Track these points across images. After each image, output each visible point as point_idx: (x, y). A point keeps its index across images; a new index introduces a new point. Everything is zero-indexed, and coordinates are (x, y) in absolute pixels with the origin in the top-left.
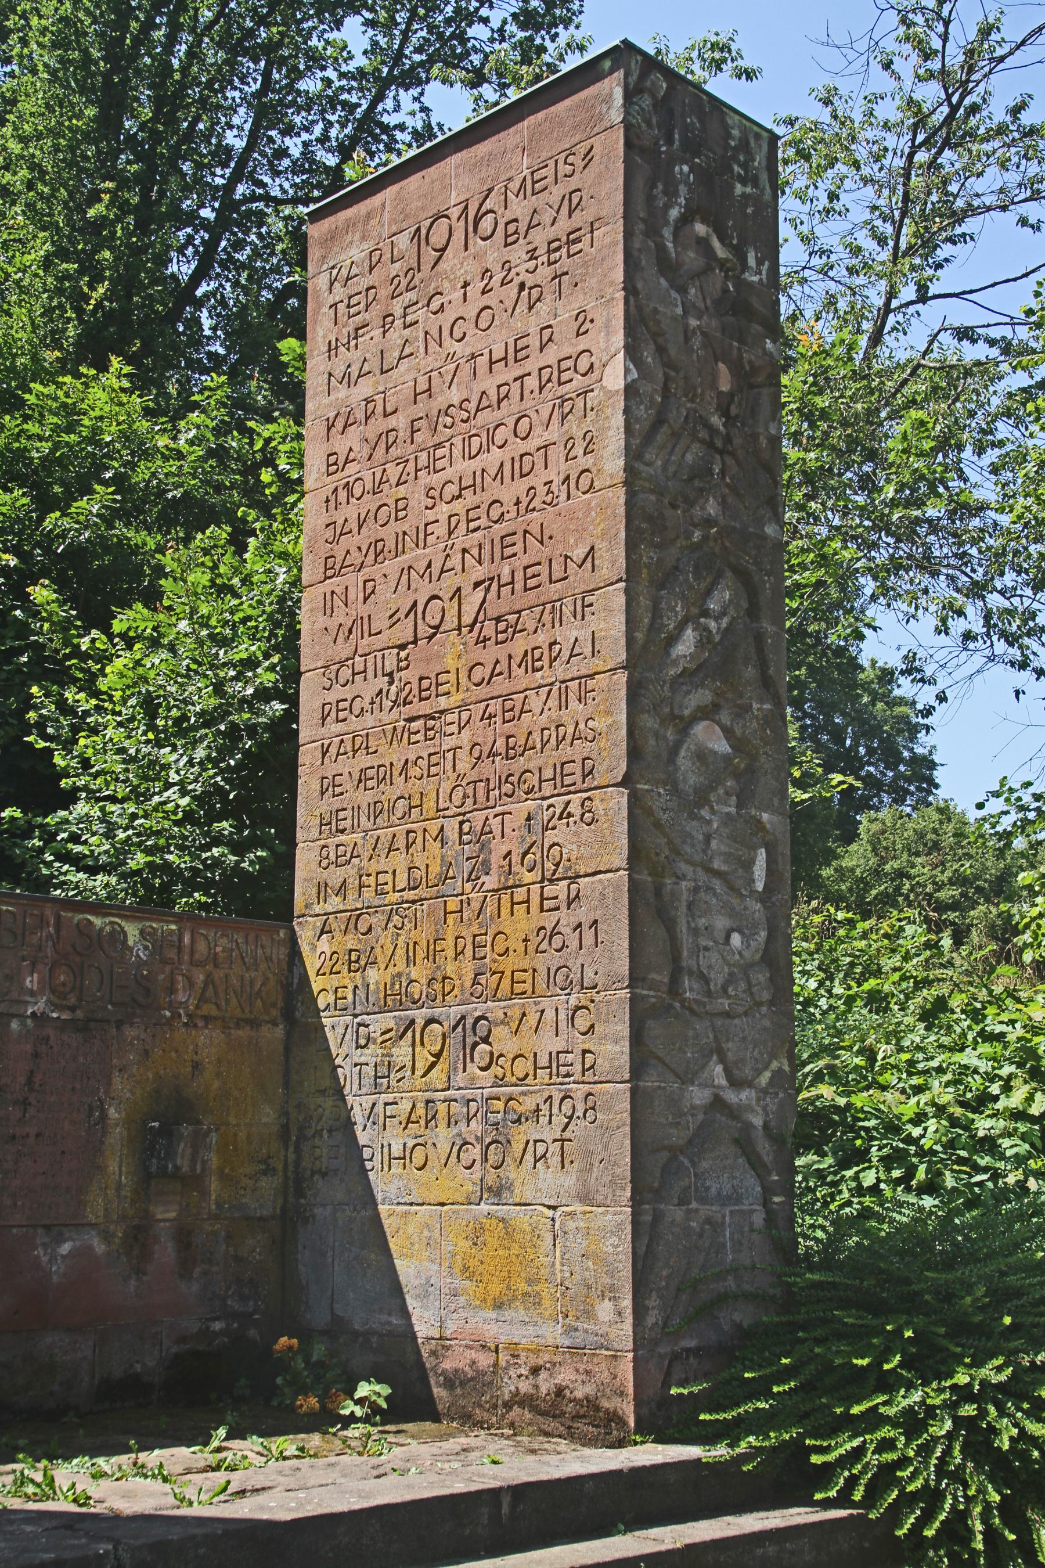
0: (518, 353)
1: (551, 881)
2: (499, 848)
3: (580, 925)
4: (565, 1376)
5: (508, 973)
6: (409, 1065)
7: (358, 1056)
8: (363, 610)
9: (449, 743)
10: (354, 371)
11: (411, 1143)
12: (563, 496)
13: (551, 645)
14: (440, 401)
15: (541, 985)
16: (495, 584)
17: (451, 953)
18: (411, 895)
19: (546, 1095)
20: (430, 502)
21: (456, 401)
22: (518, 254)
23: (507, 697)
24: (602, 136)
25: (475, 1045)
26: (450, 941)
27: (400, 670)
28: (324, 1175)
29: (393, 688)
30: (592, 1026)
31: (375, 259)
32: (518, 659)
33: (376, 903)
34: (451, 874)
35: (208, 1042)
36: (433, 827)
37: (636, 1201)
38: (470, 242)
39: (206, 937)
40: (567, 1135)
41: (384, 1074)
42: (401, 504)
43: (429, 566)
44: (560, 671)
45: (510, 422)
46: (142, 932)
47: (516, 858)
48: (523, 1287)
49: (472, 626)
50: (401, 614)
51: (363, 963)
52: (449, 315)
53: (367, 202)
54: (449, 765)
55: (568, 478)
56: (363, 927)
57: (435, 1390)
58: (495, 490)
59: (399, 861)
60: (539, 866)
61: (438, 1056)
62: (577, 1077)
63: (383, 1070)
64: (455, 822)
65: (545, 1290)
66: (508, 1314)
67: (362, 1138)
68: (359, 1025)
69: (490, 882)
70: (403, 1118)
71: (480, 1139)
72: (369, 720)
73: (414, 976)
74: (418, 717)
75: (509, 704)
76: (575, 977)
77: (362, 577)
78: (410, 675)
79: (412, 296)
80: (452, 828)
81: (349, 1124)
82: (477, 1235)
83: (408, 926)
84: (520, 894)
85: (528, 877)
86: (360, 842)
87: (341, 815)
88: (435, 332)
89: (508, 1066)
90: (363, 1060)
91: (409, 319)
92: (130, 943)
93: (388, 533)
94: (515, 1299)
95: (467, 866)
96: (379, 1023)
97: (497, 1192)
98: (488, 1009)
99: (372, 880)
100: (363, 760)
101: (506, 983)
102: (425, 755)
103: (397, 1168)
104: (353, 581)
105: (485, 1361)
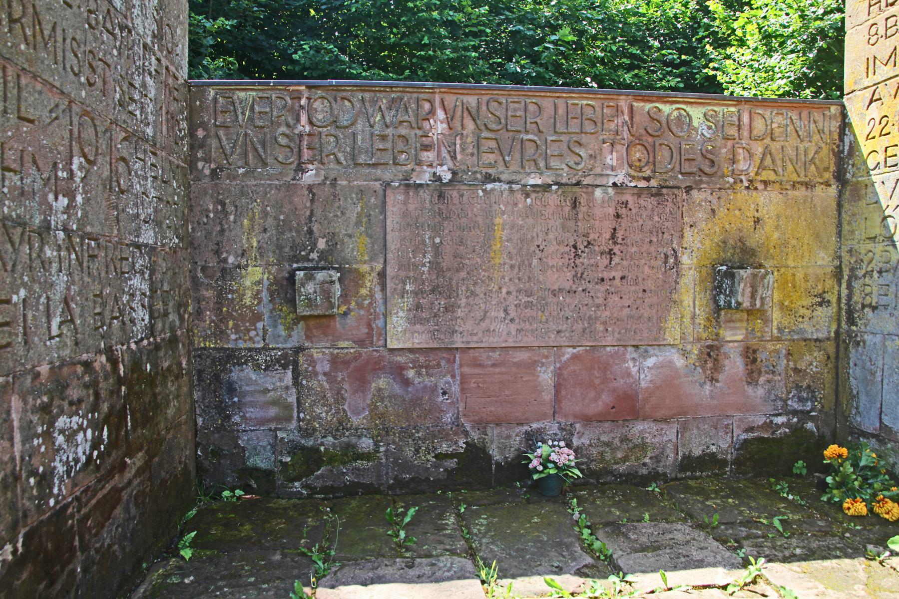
35: (768, 202)
92: (695, 124)
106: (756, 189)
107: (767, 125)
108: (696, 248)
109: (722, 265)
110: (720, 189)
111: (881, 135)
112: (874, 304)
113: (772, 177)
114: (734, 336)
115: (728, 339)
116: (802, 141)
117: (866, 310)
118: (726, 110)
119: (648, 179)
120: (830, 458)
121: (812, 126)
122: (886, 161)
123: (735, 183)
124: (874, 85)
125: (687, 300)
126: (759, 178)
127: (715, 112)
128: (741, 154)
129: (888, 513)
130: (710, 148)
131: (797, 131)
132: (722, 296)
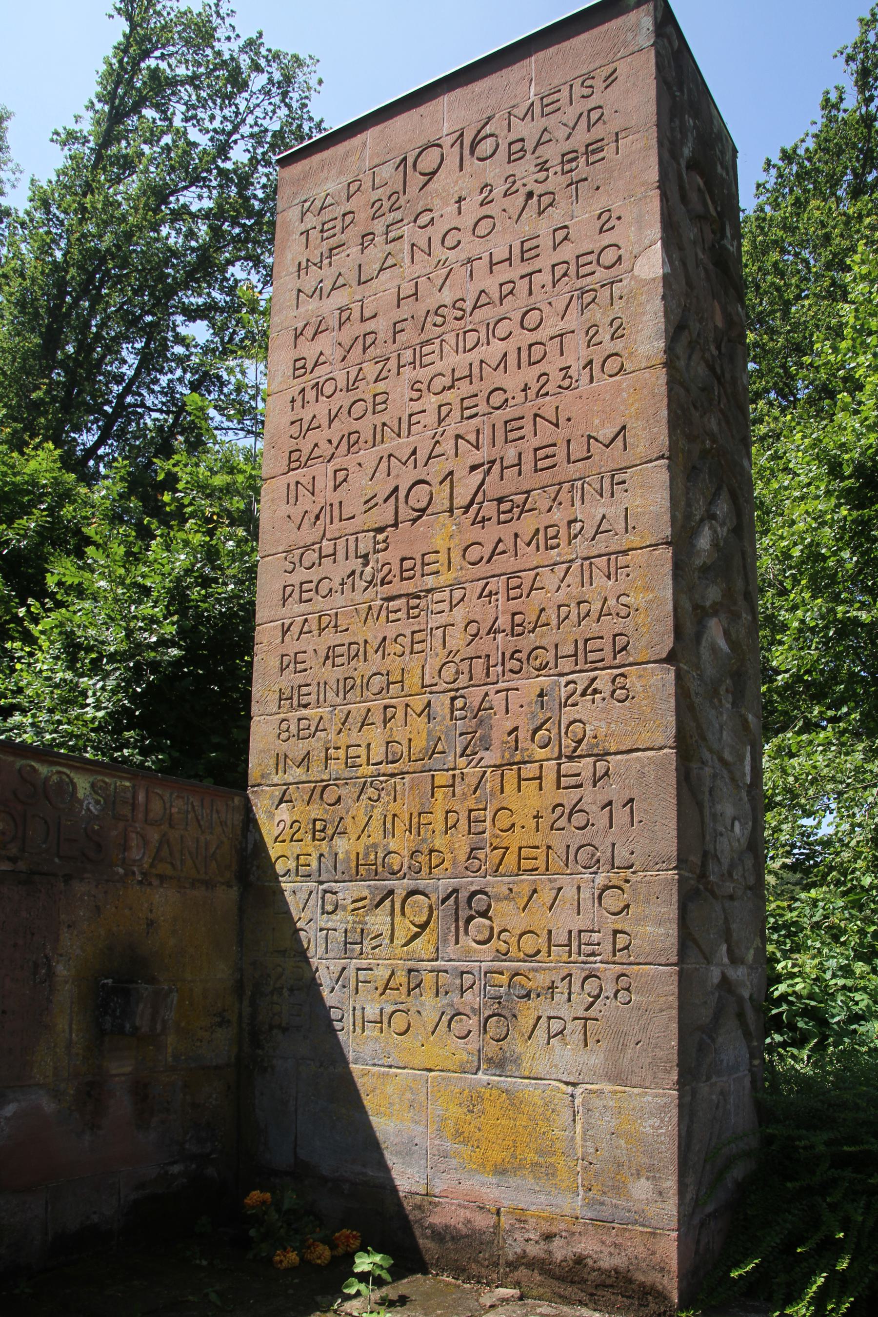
0: (527, 251)
1: (570, 758)
2: (501, 724)
3: (610, 803)
4: (586, 1246)
5: (514, 849)
6: (387, 934)
7: (323, 921)
8: (334, 498)
9: (435, 621)
10: (327, 285)
11: (389, 1009)
12: (585, 378)
13: (570, 523)
14: (431, 303)
15: (557, 863)
16: (497, 467)
17: (440, 826)
18: (391, 768)
19: (565, 972)
20: (415, 395)
21: (448, 301)
22: (526, 169)
23: (513, 574)
24: (629, 59)
25: (470, 919)
26: (439, 815)
27: (376, 551)
28: (285, 1030)
29: (368, 569)
30: (627, 906)
31: (352, 189)
32: (527, 539)
33: (346, 775)
34: (439, 748)
35: (164, 902)
36: (418, 703)
37: (681, 1084)
38: (466, 163)
39: (161, 797)
40: (592, 1013)
41: (354, 941)
42: (379, 399)
43: (414, 453)
44: (581, 547)
45: (517, 316)
46: (93, 786)
47: (523, 734)
48: (532, 1157)
49: (467, 508)
50: (379, 499)
51: (330, 832)
52: (441, 227)
53: (346, 143)
54: (437, 643)
55: (590, 362)
56: (330, 796)
57: (421, 1241)
58: (498, 379)
59: (376, 735)
60: (554, 742)
61: (423, 927)
62: (607, 955)
63: (354, 937)
64: (446, 699)
65: (561, 1163)
66: (513, 1181)
67: (329, 999)
68: (326, 891)
69: (491, 757)
70: (381, 984)
71: (477, 1012)
72: (338, 600)
73: (392, 846)
74: (400, 596)
75: (514, 582)
76: (603, 854)
77: (331, 467)
78: (392, 556)
79: (397, 215)
80: (441, 704)
81: (313, 986)
82: (474, 1102)
83: (385, 798)
84: (530, 770)
85: (540, 753)
86: (326, 717)
87: (304, 690)
88: (423, 244)
89: (514, 940)
90: (330, 925)
91: (391, 235)
92: (80, 795)
93: (365, 427)
94: (521, 1167)
95: (460, 742)
96: (347, 892)
97: (499, 1064)
98: (487, 884)
99: (341, 753)
100: (330, 638)
101: (511, 859)
102: (408, 633)
103: (371, 1031)
104: (323, 473)
105: (482, 1221)
106: (150, 884)
107: (165, 809)
108: (72, 955)
109: (107, 978)
110: (107, 881)
111: (291, 841)
112: (284, 1025)
113: (169, 871)
114: (120, 1068)
115: (114, 1072)
116: (203, 832)
117: (275, 1031)
118: (118, 783)
119: (13, 860)
120: (253, 1207)
121: (215, 816)
122: (297, 870)
123: (126, 874)
124: (284, 784)
125: (62, 1023)
126: (154, 871)
127: (106, 783)
128: (134, 840)
129: (319, 1258)
130: (96, 827)
131: (198, 821)
132: (108, 1018)
